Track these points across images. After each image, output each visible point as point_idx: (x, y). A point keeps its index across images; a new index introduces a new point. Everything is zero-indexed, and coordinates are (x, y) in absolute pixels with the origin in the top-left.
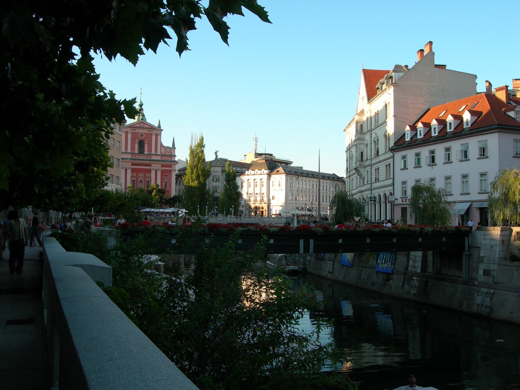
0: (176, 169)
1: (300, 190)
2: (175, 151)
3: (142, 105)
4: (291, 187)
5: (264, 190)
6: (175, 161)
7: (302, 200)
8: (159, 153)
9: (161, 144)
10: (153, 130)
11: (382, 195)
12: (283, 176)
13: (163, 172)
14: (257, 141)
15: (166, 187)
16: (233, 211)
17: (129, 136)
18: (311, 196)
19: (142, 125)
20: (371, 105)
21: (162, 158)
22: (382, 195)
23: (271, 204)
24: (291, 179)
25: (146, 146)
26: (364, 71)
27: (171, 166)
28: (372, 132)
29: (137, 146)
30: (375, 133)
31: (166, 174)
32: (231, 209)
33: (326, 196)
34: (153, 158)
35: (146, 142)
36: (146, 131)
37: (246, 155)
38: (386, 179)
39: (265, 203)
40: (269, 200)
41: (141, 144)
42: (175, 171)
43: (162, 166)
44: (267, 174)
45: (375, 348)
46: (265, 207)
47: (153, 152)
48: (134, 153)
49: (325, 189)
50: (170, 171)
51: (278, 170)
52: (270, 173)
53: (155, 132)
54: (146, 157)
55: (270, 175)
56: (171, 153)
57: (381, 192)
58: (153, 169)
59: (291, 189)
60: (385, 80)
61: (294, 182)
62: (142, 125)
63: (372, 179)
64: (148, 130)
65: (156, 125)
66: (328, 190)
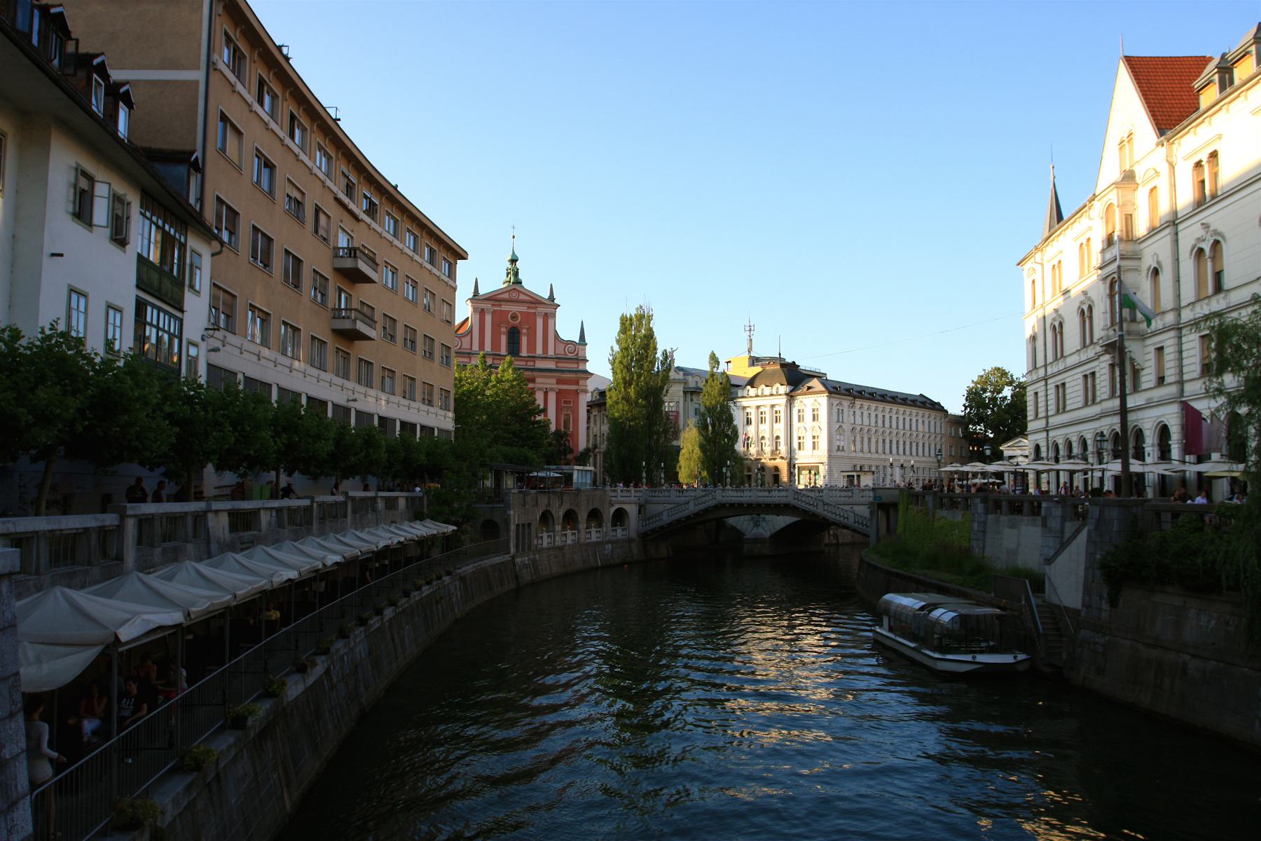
0: (588, 388)
1: (859, 428)
2: (585, 350)
3: (517, 261)
4: (838, 421)
5: (780, 429)
6: (586, 372)
7: (858, 454)
8: (551, 352)
9: (555, 337)
10: (537, 305)
11: (1074, 439)
12: (823, 400)
13: (560, 394)
14: (752, 332)
15: (566, 426)
16: (729, 474)
17: (488, 318)
18: (873, 440)
19: (514, 294)
20: (1175, 146)
21: (559, 365)
22: (1074, 439)
23: (797, 459)
24: (840, 404)
25: (524, 340)
26: (1127, 61)
27: (577, 383)
28: (1180, 227)
29: (504, 339)
30: (1202, 224)
31: (567, 400)
32: (724, 470)
33: (911, 443)
34: (540, 364)
35: (524, 331)
36: (524, 309)
37: (730, 362)
38: (1086, 404)
39: (782, 458)
40: (791, 451)
41: (514, 336)
42: (586, 391)
43: (559, 382)
44: (786, 394)
45: (920, 708)
46: (783, 465)
47: (539, 351)
48: (499, 355)
49: (907, 427)
50: (576, 393)
51: (809, 384)
52: (791, 391)
53: (541, 310)
54: (524, 363)
55: (792, 396)
56: (577, 354)
57: (1073, 433)
58: (540, 389)
59: (840, 426)
60: (1252, 45)
61: (846, 410)
62: (514, 295)
63: (1184, 368)
64: (528, 305)
65: (545, 295)
66: (914, 428)
